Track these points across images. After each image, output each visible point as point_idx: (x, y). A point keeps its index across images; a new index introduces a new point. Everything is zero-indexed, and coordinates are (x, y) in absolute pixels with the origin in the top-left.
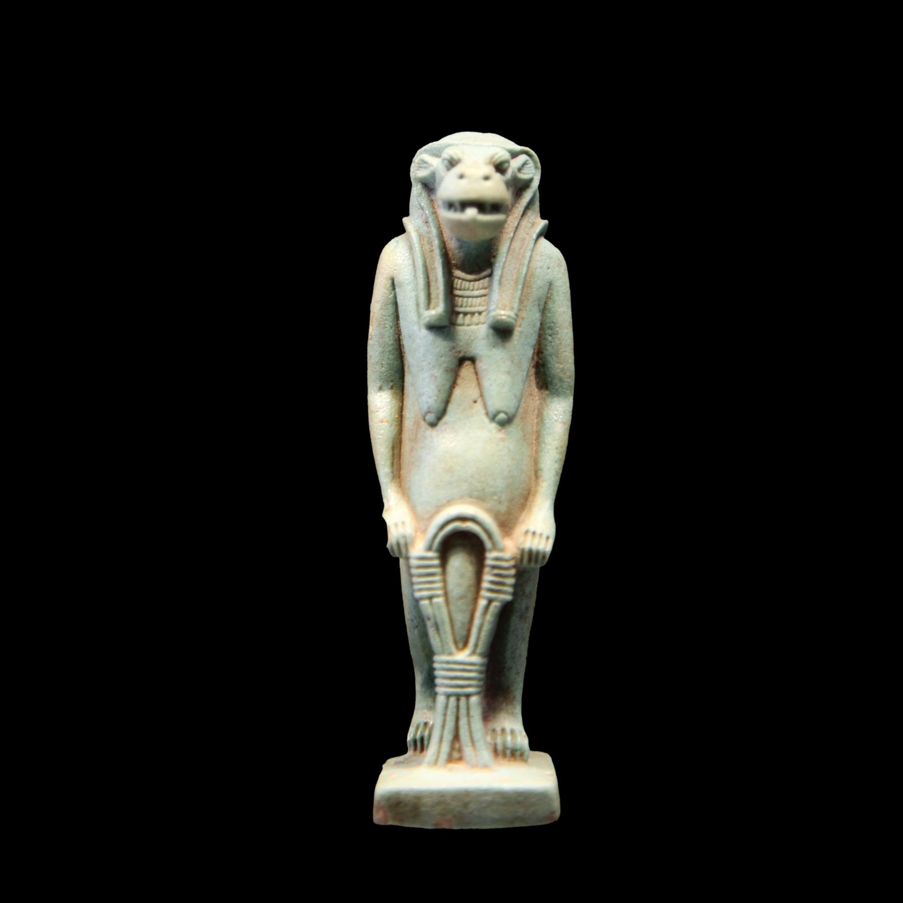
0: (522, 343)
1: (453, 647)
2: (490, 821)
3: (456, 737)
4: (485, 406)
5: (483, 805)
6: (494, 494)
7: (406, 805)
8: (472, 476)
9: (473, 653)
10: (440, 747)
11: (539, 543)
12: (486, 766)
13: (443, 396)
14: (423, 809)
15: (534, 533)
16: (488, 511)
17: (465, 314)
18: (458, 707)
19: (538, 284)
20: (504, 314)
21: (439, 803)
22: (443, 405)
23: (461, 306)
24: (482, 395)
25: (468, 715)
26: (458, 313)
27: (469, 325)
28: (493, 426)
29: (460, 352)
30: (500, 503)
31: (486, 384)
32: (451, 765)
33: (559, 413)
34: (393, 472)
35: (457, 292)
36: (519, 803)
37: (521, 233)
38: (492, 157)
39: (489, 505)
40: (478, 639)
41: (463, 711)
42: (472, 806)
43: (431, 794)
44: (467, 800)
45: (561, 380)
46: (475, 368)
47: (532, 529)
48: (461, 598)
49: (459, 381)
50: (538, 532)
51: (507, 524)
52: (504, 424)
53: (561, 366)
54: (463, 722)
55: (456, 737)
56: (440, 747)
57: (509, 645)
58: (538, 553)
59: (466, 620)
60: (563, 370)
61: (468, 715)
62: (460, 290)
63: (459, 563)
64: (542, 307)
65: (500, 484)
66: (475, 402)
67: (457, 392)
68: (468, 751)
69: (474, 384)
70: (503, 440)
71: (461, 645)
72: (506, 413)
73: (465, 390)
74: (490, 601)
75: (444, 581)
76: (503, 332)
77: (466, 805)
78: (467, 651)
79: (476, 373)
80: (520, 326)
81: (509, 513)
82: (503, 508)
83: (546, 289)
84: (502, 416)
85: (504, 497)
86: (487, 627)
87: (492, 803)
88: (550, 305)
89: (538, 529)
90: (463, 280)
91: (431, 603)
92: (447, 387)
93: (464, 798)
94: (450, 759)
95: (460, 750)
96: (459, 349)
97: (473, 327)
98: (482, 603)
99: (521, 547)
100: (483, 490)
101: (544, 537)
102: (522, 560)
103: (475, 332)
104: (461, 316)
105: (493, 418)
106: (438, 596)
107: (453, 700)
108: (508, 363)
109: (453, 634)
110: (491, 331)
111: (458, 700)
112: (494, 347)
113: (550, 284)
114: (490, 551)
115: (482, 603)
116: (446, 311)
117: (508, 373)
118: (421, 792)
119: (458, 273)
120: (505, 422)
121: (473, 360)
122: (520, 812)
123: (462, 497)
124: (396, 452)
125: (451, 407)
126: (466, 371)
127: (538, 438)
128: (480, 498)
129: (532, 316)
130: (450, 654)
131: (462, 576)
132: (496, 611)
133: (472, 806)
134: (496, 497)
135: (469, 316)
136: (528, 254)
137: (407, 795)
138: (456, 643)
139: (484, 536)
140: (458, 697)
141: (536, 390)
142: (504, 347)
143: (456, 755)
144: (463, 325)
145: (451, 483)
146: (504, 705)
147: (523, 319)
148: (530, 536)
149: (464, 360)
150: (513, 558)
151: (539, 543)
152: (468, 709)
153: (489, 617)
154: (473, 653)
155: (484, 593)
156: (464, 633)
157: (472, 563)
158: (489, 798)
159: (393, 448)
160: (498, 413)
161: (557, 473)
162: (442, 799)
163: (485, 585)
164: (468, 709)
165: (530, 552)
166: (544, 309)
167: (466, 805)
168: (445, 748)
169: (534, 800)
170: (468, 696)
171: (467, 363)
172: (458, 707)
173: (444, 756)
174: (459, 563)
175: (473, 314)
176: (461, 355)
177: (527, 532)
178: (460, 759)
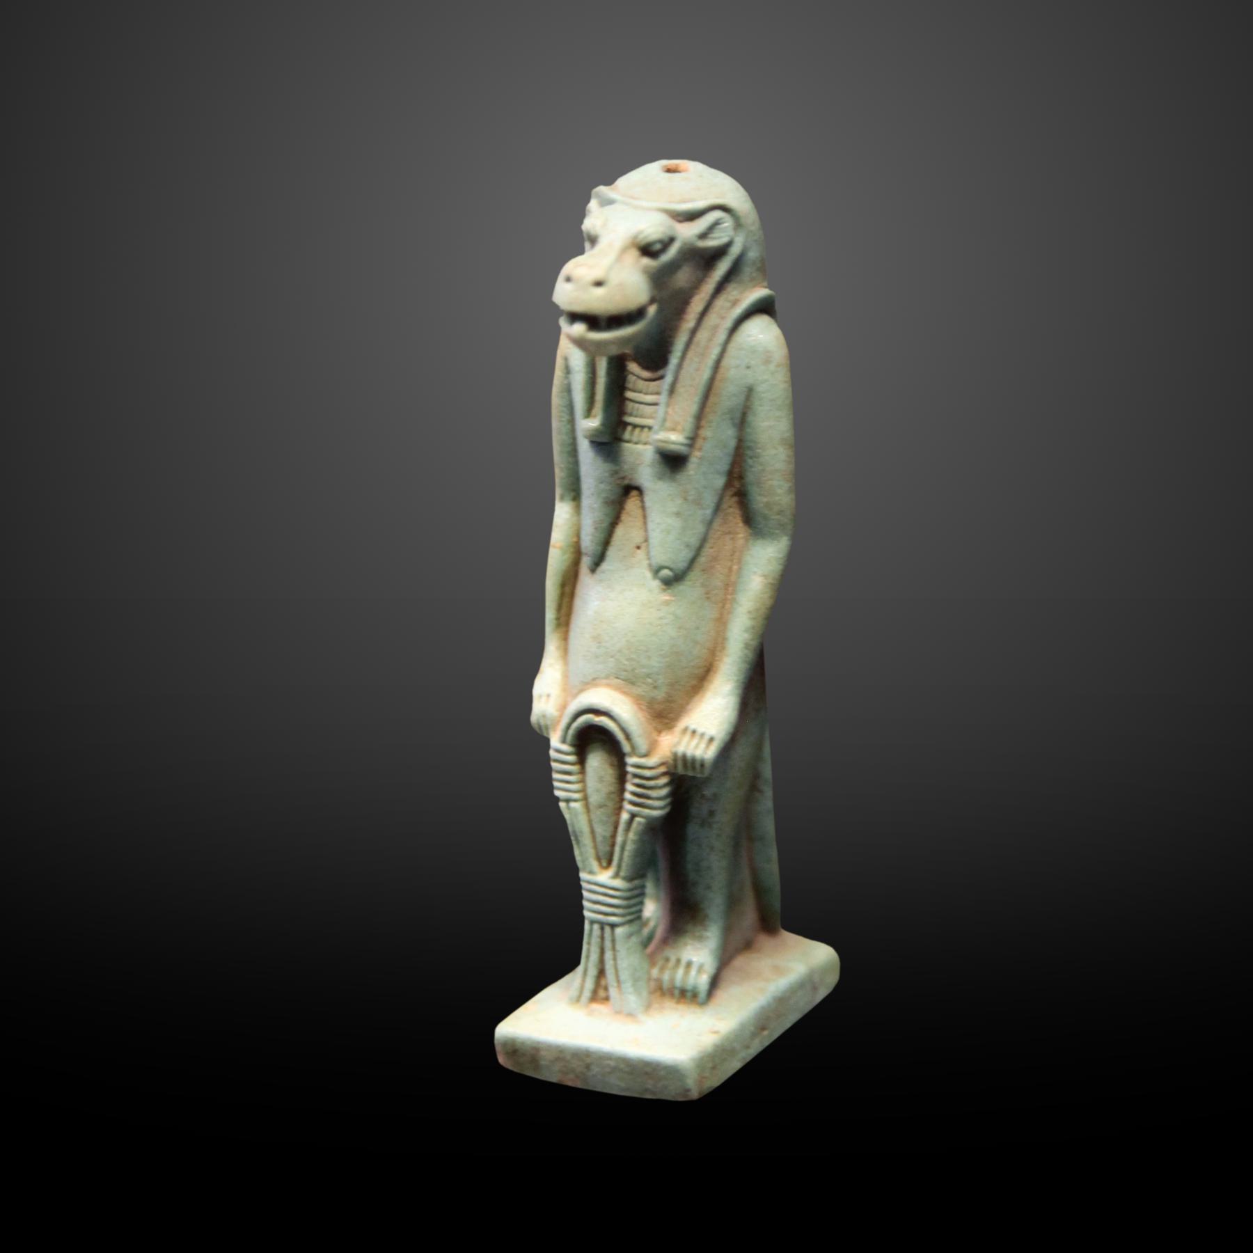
0: (705, 473)
1: (595, 865)
2: (616, 1086)
4: (648, 553)
5: (608, 1070)
6: (648, 676)
7: (524, 1055)
8: (620, 651)
9: (616, 875)
10: (584, 981)
11: (697, 747)
12: (630, 1015)
13: (601, 536)
14: (543, 1063)
15: (694, 732)
16: (638, 700)
17: (635, 426)
18: (602, 938)
19: (728, 395)
20: (675, 439)
21: (558, 1059)
22: (600, 548)
23: (631, 415)
24: (646, 540)
25: (614, 948)
26: (626, 424)
27: (636, 443)
28: (656, 584)
29: (623, 478)
30: (655, 687)
31: (651, 526)
32: (595, 1006)
35: (629, 394)
36: (646, 1073)
37: (712, 319)
38: (636, 237)
39: (639, 691)
40: (621, 859)
41: (608, 944)
42: (595, 1070)
43: (550, 1047)
44: (588, 1061)
45: (765, 518)
46: (642, 501)
47: (693, 727)
48: (601, 806)
49: (624, 517)
50: (700, 730)
51: (665, 714)
52: (668, 583)
53: (765, 500)
54: (608, 955)
55: (601, 973)
56: (584, 981)
57: (689, 857)
58: (694, 760)
59: (608, 834)
60: (768, 505)
61: (614, 948)
62: (634, 391)
63: (597, 761)
64: (737, 421)
65: (656, 663)
66: (638, 548)
67: (620, 531)
68: (613, 992)
69: (639, 523)
70: (667, 603)
71: (605, 864)
72: (671, 569)
73: (626, 532)
74: (633, 816)
75: (583, 781)
76: (673, 462)
77: (588, 1067)
78: (610, 872)
79: (643, 508)
80: (700, 449)
81: (669, 700)
82: (660, 695)
83: (742, 398)
84: (665, 572)
85: (661, 680)
86: (630, 847)
87: (614, 1070)
88: (750, 418)
89: (711, 718)
90: (638, 377)
91: (568, 808)
92: (605, 525)
93: (585, 1057)
94: (594, 998)
95: (606, 989)
96: (622, 474)
97: (640, 447)
98: (625, 816)
99: (674, 750)
100: (633, 670)
101: (707, 738)
102: (675, 766)
103: (640, 454)
104: (629, 428)
105: (656, 571)
106: (575, 801)
107: (596, 927)
108: (679, 501)
109: (595, 847)
110: (657, 456)
111: (602, 929)
112: (660, 479)
113: (750, 391)
114: (630, 755)
115: (625, 816)
116: (604, 424)
117: (678, 514)
118: (539, 1043)
119: (633, 367)
120: (673, 580)
121: (639, 489)
122: (650, 1084)
123: (607, 677)
124: (567, 589)
125: (611, 552)
126: (632, 504)
127: (730, 588)
128: (628, 680)
129: (720, 436)
131: (601, 779)
132: (641, 828)
133: (595, 1070)
134: (650, 681)
135: (637, 430)
136: (715, 351)
137: (523, 1043)
138: (599, 859)
139: (620, 736)
141: (741, 525)
142: (673, 479)
143: (602, 993)
144: (628, 442)
145: (597, 657)
146: (690, 927)
147: (704, 439)
148: (687, 737)
149: (627, 490)
150: (663, 764)
151: (697, 747)
152: (613, 941)
153: (631, 835)
154: (616, 875)
155: (628, 806)
156: (608, 849)
157: (612, 765)
158: (612, 1063)
160: (661, 568)
161: (747, 646)
162: (562, 1055)
163: (628, 796)
164: (613, 941)
165: (684, 757)
166: (742, 419)
167: (588, 1067)
168: (590, 984)
169: (662, 1073)
170: (613, 926)
171: (634, 493)
172: (602, 938)
173: (587, 993)
174: (597, 761)
175: (642, 427)
176: (626, 482)
177: (685, 730)
178: (607, 999)
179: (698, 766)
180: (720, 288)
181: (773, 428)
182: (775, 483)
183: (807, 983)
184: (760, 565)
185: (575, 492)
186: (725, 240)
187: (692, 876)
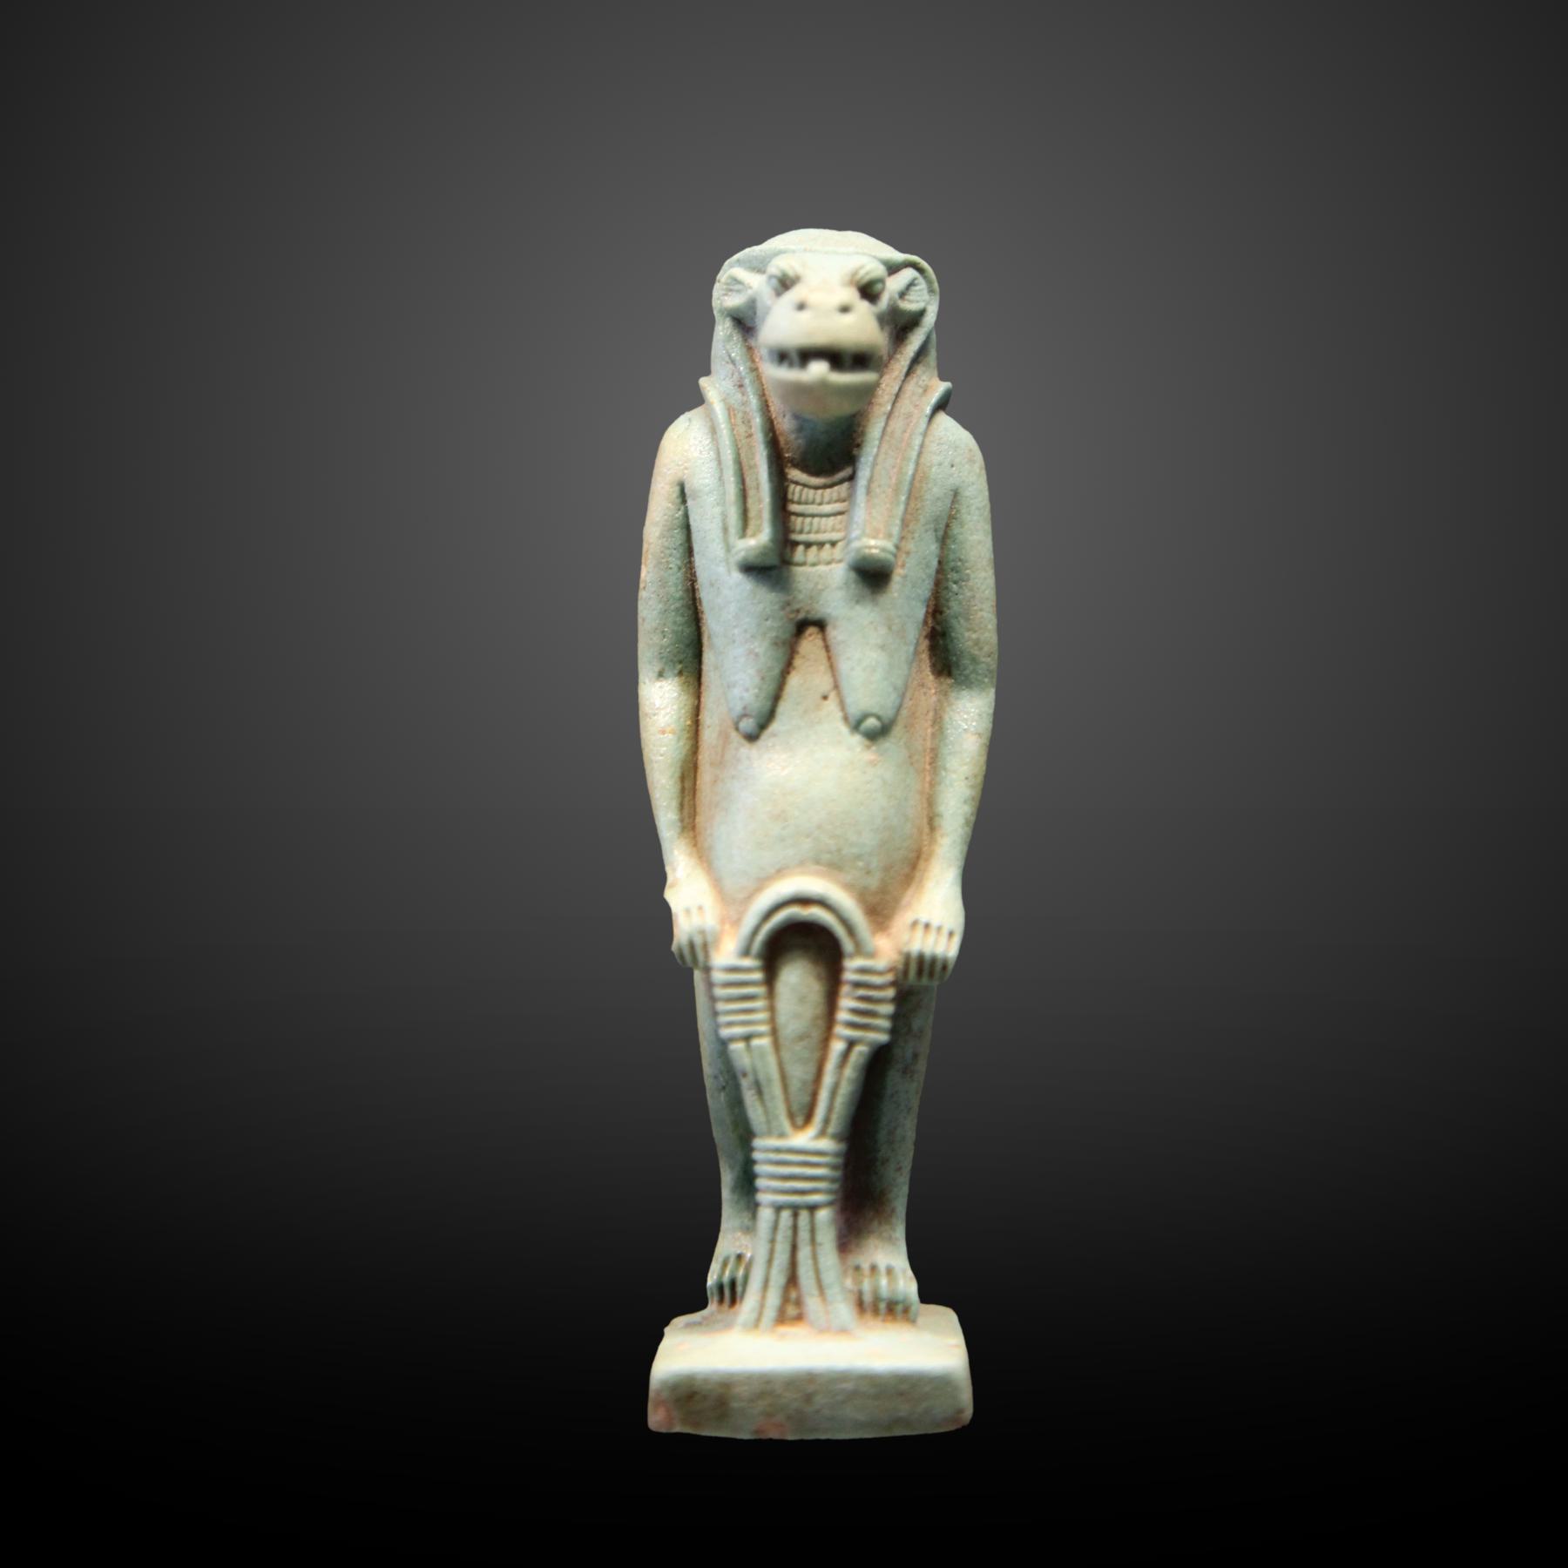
0: (907, 596)
1: (786, 1124)
2: (851, 1425)
3: (792, 1279)
4: (842, 705)
5: (840, 1398)
6: (858, 857)
7: (705, 1397)
8: (819, 827)
9: (822, 1133)
10: (763, 1297)
11: (936, 942)
12: (843, 1331)
13: (770, 688)
14: (735, 1405)
15: (927, 926)
16: (848, 887)
17: (808, 545)
18: (795, 1228)
19: (935, 493)
20: (875, 545)
21: (762, 1395)
22: (769, 704)
23: (801, 532)
24: (836, 686)
25: (813, 1241)
26: (796, 544)
27: (814, 565)
28: (857, 739)
29: (798, 611)
30: (868, 873)
31: (844, 666)
32: (783, 1329)
34: (682, 820)
35: (794, 508)
36: (901, 1394)
37: (905, 405)
38: (855, 273)
39: (848, 878)
40: (830, 1109)
41: (804, 1235)
42: (820, 1400)
43: (749, 1378)
44: (811, 1388)
45: (974, 660)
46: (824, 640)
47: (924, 918)
48: (801, 1038)
49: (797, 662)
50: (935, 923)
51: (880, 910)
52: (876, 736)
53: (974, 636)
54: (804, 1253)
55: (792, 1279)
56: (763, 1297)
57: (885, 1120)
58: (934, 960)
59: (810, 1077)
60: (977, 643)
61: (813, 1241)
62: (799, 503)
63: (797, 977)
64: (941, 533)
65: (868, 840)
66: (825, 698)
67: (794, 681)
68: (812, 1303)
69: (823, 666)
70: (873, 763)
71: (800, 1120)
72: (879, 718)
73: (808, 678)
74: (851, 1044)
75: (772, 1009)
76: (873, 576)
77: (808, 1398)
78: (812, 1131)
79: (827, 648)
80: (903, 566)
81: (883, 890)
82: (873, 882)
83: (948, 502)
84: (871, 722)
85: (875, 863)
86: (845, 1089)
87: (854, 1394)
88: (955, 530)
89: (934, 918)
90: (805, 485)
91: (748, 1047)
92: (777, 671)
93: (806, 1385)
94: (782, 1318)
95: (799, 1303)
96: (796, 606)
97: (822, 568)
98: (838, 1046)
99: (905, 949)
100: (839, 850)
101: (945, 932)
102: (906, 972)
103: (824, 577)
104: (801, 548)
105: (856, 726)
106: (760, 1035)
107: (786, 1215)
108: (883, 631)
109: (787, 1100)
110: (853, 575)
111: (795, 1215)
112: (857, 602)
113: (956, 494)
114: (851, 956)
115: (838, 1046)
116: (774, 540)
117: (883, 647)
118: (732, 1375)
119: (795, 474)
120: (878, 733)
121: (821, 625)
122: (904, 1409)
123: (802, 863)
124: (688, 784)
125: (783, 707)
126: (810, 644)
128: (833, 865)
129: (924, 549)
130: (782, 1135)
131: (802, 1000)
132: (862, 1060)
133: (820, 1400)
134: (860, 864)
135: (814, 549)
136: (917, 442)
137: (706, 1381)
138: (791, 1116)
139: (840, 931)
140: (795, 1210)
141: (931, 677)
142: (875, 602)
143: (791, 1311)
144: (803, 564)
145: (783, 840)
146: (875, 1223)
147: (908, 553)
148: (920, 931)
149: (806, 625)
150: (891, 970)
151: (936, 942)
152: (813, 1231)
153: (849, 1072)
154: (822, 1133)
155: (840, 1030)
156: (806, 1099)
157: (819, 978)
158: (849, 1386)
159: (683, 778)
160: (865, 716)
161: (967, 822)
162: (767, 1387)
163: (843, 1016)
164: (813, 1231)
165: (921, 959)
166: (945, 537)
167: (808, 1398)
168: (773, 1298)
169: (927, 1389)
170: (812, 1208)
171: (812, 630)
172: (795, 1228)
173: (770, 1312)
174: (797, 977)
175: (821, 545)
176: (801, 616)
177: (915, 924)
178: (799, 1318)
179: (938, 967)
181: (977, 540)
182: (985, 614)
183: (905, 1386)
184: (969, 717)
185: (690, 658)
186: (920, 306)
187: (884, 1151)
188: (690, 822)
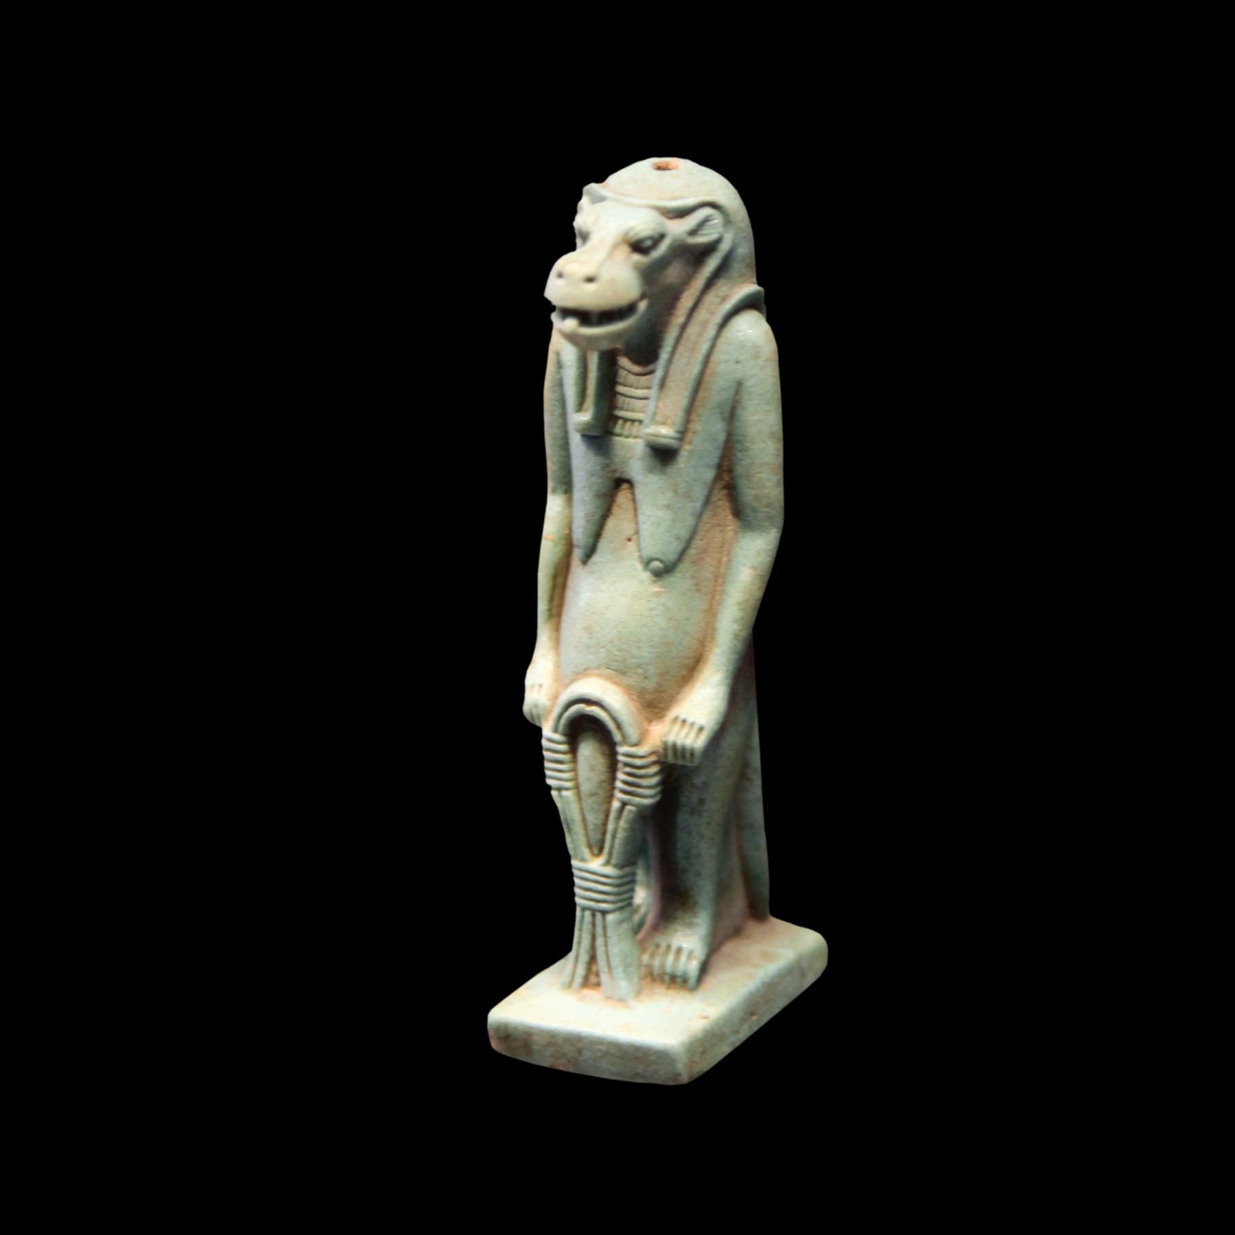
0: (695, 466)
1: (586, 852)
2: (607, 1070)
4: (639, 546)
5: (599, 1054)
6: (639, 666)
7: (516, 1039)
8: (611, 642)
9: (607, 863)
10: (575, 967)
11: (687, 736)
12: (621, 1000)
13: (592, 529)
14: (535, 1047)
15: (684, 722)
16: (629, 690)
17: (626, 420)
18: (594, 924)
19: (718, 389)
20: (665, 433)
21: (550, 1044)
22: (591, 540)
23: (622, 409)
24: (637, 533)
25: (605, 935)
26: (617, 418)
27: (627, 437)
28: (646, 576)
29: (614, 471)
30: (646, 678)
31: (641, 518)
32: (586, 992)
33: (750, 557)
35: (620, 389)
36: (637, 1058)
37: (701, 314)
38: (627, 234)
39: (629, 681)
40: (612, 847)
41: (599, 930)
42: (587, 1054)
43: (542, 1032)
44: (580, 1045)
45: (754, 510)
46: (633, 494)
47: (683, 716)
48: (592, 795)
49: (615, 509)
50: (690, 719)
51: (655, 703)
52: (658, 575)
53: (754, 493)
54: (600, 941)
55: (593, 959)
57: (679, 845)
58: (684, 749)
59: (599, 822)
60: (757, 498)
61: (605, 935)
62: (625, 385)
63: (588, 750)
64: (727, 415)
65: (646, 653)
66: (629, 540)
67: (611, 524)
68: (604, 978)
69: (630, 516)
70: (657, 594)
71: (596, 852)
72: (661, 561)
73: (617, 525)
74: (624, 804)
75: (574, 770)
76: (663, 455)
77: (579, 1051)
78: (602, 859)
79: (634, 501)
80: (690, 443)
81: (659, 690)
82: (651, 685)
83: (732, 392)
84: (656, 564)
85: (652, 670)
86: (621, 835)
87: (606, 1054)
88: (739, 412)
89: (701, 707)
90: (629, 372)
91: (560, 796)
92: (597, 517)
93: (576, 1042)
94: (586, 983)
95: (597, 974)
96: (613, 468)
97: (630, 440)
98: (616, 805)
99: (664, 739)
100: (624, 660)
101: (696, 727)
102: (666, 755)
103: (631, 447)
104: (620, 422)
105: (647, 563)
106: (567, 789)
107: (587, 913)
108: (669, 494)
109: (587, 835)
110: (648, 450)
111: (594, 916)
112: (650, 472)
113: (739, 386)
114: (621, 744)
115: (616, 805)
116: (596, 418)
117: (668, 507)
118: (531, 1028)
119: (624, 362)
120: (663, 571)
121: (630, 482)
122: (640, 1069)
123: (598, 667)
124: (559, 581)
125: (603, 544)
126: (623, 497)
128: (619, 670)
129: (709, 430)
131: (592, 768)
132: (631, 816)
133: (587, 1054)
134: (640, 671)
135: (628, 424)
136: (705, 346)
137: (515, 1028)
138: (590, 847)
139: (611, 725)
141: (730, 517)
142: (663, 472)
143: (593, 979)
144: (619, 435)
145: (588, 647)
146: (680, 913)
147: (694, 432)
148: (677, 727)
149: (618, 483)
150: (653, 753)
151: (687, 736)
152: (605, 927)
153: (622, 823)
154: (607, 863)
155: (619, 795)
156: (599, 836)
157: (603, 754)
158: (603, 1048)
160: (652, 560)
161: (736, 637)
162: (554, 1039)
163: (619, 784)
164: (605, 927)
165: (674, 746)
166: (731, 413)
167: (579, 1051)
168: (581, 970)
169: (653, 1057)
170: (604, 913)
171: (625, 486)
172: (594, 924)
173: (579, 979)
174: (588, 750)
175: (633, 421)
176: (617, 475)
177: (676, 719)
178: (598, 984)
179: (688, 755)
180: (709, 284)
182: (764, 476)
186: (714, 236)
187: (682, 863)
188: (557, 612)
